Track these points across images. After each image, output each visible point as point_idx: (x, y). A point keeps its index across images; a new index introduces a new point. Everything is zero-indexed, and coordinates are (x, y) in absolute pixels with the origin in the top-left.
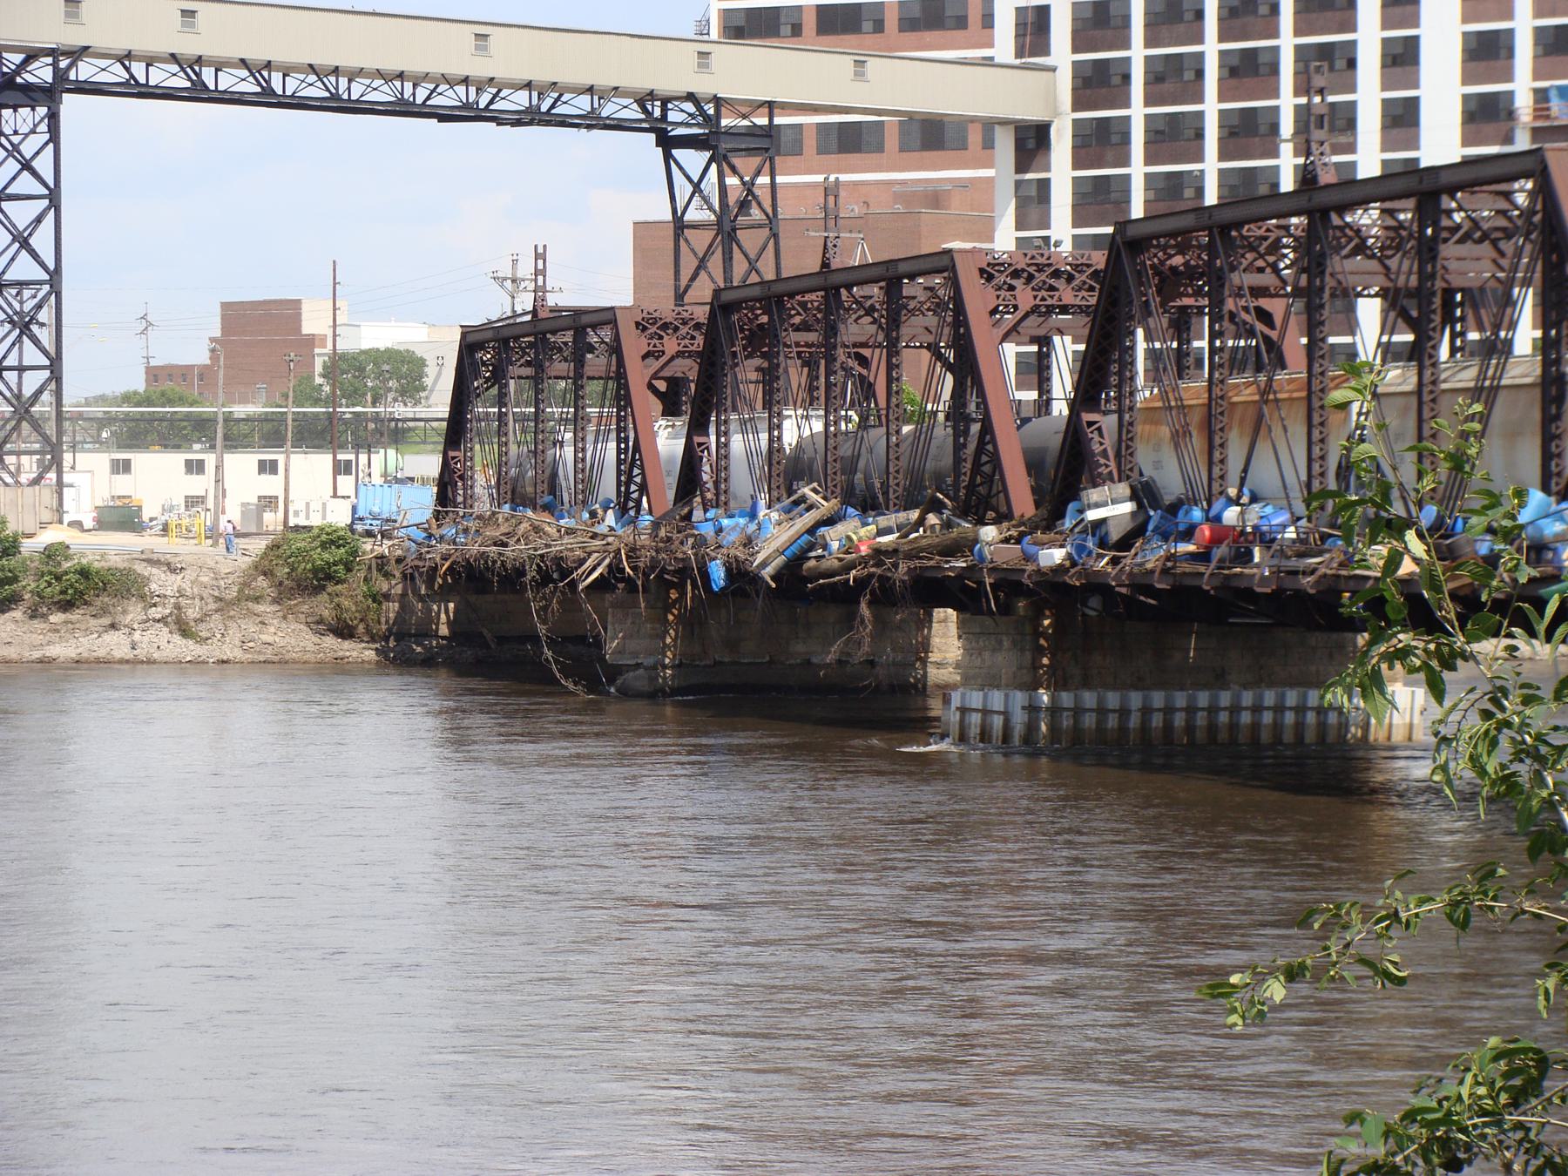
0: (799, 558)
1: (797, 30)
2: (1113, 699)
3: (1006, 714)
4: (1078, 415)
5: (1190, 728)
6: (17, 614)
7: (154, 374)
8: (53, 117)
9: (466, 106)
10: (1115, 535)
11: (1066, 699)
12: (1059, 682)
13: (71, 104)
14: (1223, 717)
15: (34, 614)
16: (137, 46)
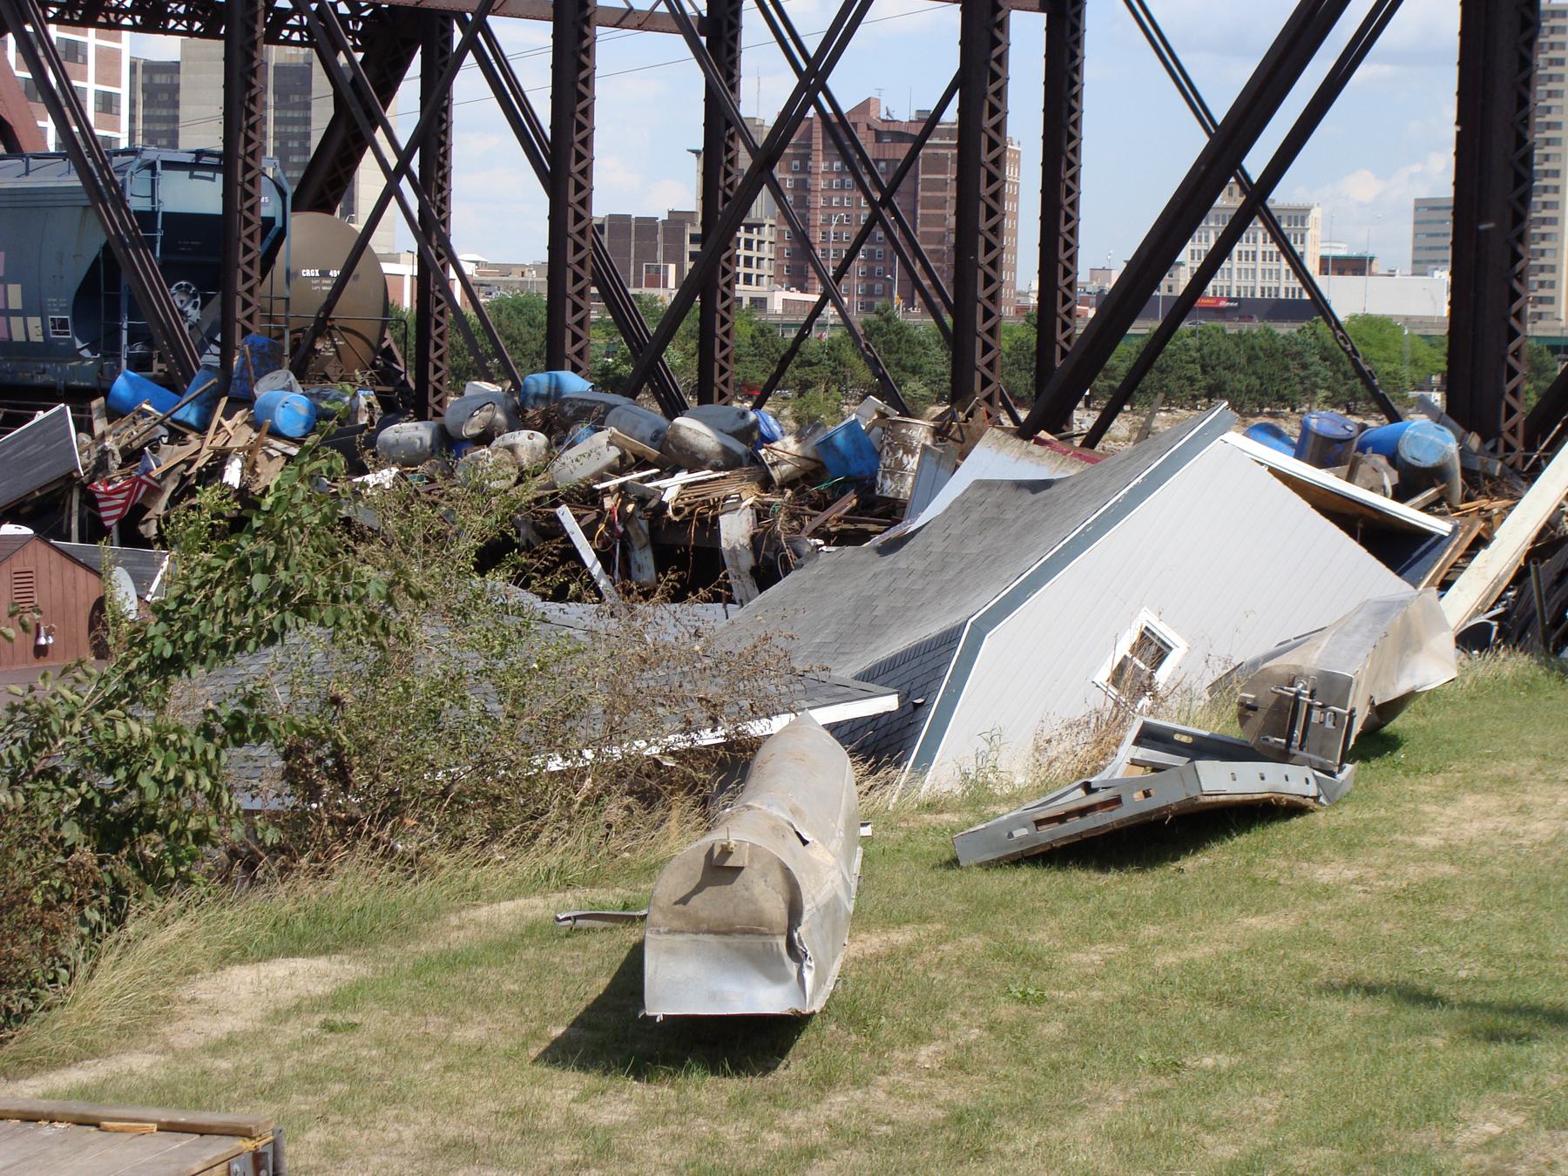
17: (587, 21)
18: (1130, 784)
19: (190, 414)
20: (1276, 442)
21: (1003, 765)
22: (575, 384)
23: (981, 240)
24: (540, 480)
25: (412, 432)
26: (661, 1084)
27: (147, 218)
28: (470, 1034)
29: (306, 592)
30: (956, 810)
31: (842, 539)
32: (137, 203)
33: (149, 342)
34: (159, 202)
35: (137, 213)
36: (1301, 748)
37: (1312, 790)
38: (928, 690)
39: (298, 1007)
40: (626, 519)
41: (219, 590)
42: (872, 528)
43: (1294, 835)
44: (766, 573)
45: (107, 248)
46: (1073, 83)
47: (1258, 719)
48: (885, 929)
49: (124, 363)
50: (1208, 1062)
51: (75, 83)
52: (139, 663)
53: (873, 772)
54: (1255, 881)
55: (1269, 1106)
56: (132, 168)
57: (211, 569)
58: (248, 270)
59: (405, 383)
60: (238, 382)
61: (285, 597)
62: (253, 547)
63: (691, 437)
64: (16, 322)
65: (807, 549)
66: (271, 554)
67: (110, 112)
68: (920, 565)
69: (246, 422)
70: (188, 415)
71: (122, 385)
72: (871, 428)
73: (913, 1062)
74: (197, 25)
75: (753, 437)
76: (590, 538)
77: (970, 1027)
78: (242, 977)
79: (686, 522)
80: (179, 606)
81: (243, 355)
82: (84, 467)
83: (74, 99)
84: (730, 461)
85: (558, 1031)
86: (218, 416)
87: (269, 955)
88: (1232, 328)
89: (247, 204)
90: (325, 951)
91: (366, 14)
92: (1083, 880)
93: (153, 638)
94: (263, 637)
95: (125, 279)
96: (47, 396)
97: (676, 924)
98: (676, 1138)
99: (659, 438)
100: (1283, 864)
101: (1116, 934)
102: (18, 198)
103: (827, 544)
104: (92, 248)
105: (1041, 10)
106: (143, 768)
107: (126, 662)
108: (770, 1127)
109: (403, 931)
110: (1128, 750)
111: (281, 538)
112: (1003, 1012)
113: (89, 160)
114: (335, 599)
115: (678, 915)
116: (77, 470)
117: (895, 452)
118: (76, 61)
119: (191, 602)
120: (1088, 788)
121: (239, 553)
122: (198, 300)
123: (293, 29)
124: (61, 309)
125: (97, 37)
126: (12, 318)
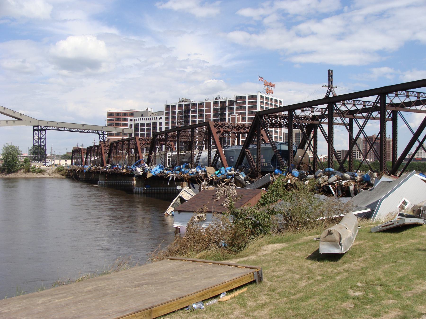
0: (90, 169)
1: (114, 125)
2: (112, 182)
3: (103, 183)
5: (119, 184)
6: (35, 173)
7: (67, 153)
8: (46, 132)
9: (70, 130)
10: (109, 168)
11: (108, 182)
12: (107, 180)
13: (47, 130)
14: (121, 183)
15: (37, 173)
16: (53, 126)
17: (332, 124)
18: (396, 221)
20: (423, 175)
21: (381, 218)
22: (331, 169)
23: (383, 150)
24: (327, 182)
25: (311, 176)
26: (322, 263)
27: (279, 150)
28: (297, 255)
30: (374, 225)
31: (366, 189)
32: (278, 149)
33: (280, 166)
36: (421, 216)
37: (423, 222)
38: (374, 208)
39: (276, 251)
40: (338, 186)
41: (269, 194)
42: (369, 187)
43: (420, 228)
44: (356, 194)
45: (275, 154)
46: (396, 130)
47: (415, 212)
48: (359, 241)
50: (401, 261)
53: (362, 219)
54: (413, 235)
55: (408, 268)
57: (269, 192)
59: (312, 170)
61: (278, 195)
62: (274, 189)
63: (346, 176)
65: (361, 190)
68: (374, 192)
71: (276, 171)
72: (369, 175)
73: (358, 260)
75: (354, 176)
76: (333, 189)
77: (367, 255)
78: (270, 246)
79: (345, 187)
84: (351, 179)
85: (310, 255)
87: (275, 243)
88: (422, 162)
90: (283, 243)
92: (389, 234)
95: (277, 158)
96: (267, 172)
97: (324, 240)
98: (321, 271)
99: (342, 176)
100: (417, 232)
101: (391, 242)
103: (363, 190)
104: (273, 154)
105: (392, 121)
106: (259, 218)
107: (257, 204)
108: (335, 269)
109: (294, 240)
110: (397, 217)
112: (373, 253)
115: (325, 239)
117: (372, 178)
120: (391, 221)
123: (298, 127)
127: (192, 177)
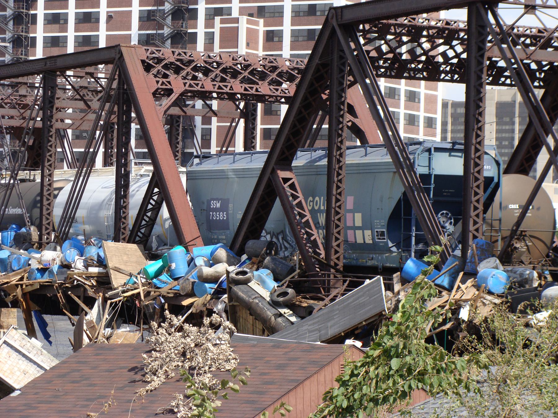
4: (273, 172)
19: (445, 281)
27: (425, 178)
29: (422, 368)
32: (421, 170)
34: (433, 169)
35: (421, 175)
45: (404, 194)
49: (413, 254)
51: (391, 109)
52: (329, 411)
56: (419, 152)
58: (476, 204)
60: (469, 264)
61: (410, 371)
64: (359, 233)
66: (401, 346)
67: (414, 125)
69: (473, 285)
70: (443, 281)
71: (410, 265)
74: (456, 76)
80: (351, 378)
81: (472, 250)
82: (388, 309)
83: (391, 118)
86: (458, 282)
89: (476, 169)
91: (546, 68)
93: (337, 396)
94: (399, 394)
96: (372, 271)
102: (361, 168)
111: (406, 335)
113: (396, 148)
114: (438, 372)
116: (385, 310)
118: (394, 98)
119: (357, 375)
121: (383, 346)
122: (452, 221)
123: (507, 77)
124: (382, 225)
125: (406, 85)
126: (357, 231)
127: (43, 287)
